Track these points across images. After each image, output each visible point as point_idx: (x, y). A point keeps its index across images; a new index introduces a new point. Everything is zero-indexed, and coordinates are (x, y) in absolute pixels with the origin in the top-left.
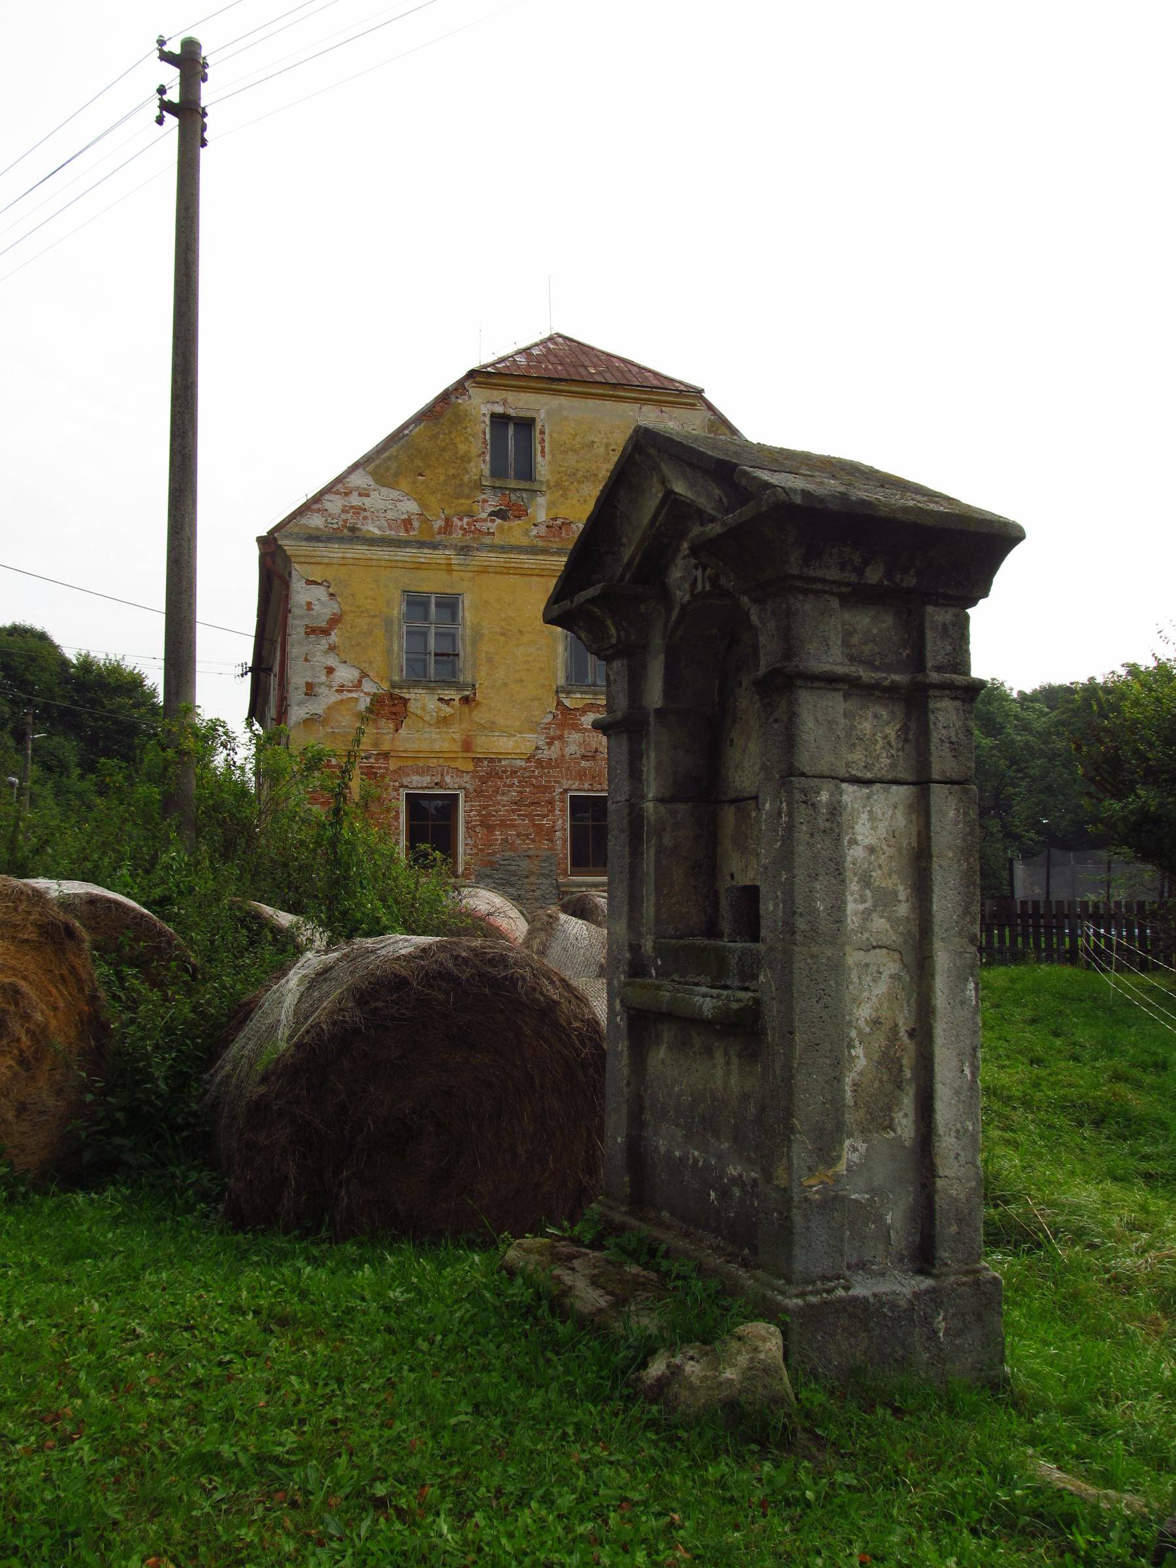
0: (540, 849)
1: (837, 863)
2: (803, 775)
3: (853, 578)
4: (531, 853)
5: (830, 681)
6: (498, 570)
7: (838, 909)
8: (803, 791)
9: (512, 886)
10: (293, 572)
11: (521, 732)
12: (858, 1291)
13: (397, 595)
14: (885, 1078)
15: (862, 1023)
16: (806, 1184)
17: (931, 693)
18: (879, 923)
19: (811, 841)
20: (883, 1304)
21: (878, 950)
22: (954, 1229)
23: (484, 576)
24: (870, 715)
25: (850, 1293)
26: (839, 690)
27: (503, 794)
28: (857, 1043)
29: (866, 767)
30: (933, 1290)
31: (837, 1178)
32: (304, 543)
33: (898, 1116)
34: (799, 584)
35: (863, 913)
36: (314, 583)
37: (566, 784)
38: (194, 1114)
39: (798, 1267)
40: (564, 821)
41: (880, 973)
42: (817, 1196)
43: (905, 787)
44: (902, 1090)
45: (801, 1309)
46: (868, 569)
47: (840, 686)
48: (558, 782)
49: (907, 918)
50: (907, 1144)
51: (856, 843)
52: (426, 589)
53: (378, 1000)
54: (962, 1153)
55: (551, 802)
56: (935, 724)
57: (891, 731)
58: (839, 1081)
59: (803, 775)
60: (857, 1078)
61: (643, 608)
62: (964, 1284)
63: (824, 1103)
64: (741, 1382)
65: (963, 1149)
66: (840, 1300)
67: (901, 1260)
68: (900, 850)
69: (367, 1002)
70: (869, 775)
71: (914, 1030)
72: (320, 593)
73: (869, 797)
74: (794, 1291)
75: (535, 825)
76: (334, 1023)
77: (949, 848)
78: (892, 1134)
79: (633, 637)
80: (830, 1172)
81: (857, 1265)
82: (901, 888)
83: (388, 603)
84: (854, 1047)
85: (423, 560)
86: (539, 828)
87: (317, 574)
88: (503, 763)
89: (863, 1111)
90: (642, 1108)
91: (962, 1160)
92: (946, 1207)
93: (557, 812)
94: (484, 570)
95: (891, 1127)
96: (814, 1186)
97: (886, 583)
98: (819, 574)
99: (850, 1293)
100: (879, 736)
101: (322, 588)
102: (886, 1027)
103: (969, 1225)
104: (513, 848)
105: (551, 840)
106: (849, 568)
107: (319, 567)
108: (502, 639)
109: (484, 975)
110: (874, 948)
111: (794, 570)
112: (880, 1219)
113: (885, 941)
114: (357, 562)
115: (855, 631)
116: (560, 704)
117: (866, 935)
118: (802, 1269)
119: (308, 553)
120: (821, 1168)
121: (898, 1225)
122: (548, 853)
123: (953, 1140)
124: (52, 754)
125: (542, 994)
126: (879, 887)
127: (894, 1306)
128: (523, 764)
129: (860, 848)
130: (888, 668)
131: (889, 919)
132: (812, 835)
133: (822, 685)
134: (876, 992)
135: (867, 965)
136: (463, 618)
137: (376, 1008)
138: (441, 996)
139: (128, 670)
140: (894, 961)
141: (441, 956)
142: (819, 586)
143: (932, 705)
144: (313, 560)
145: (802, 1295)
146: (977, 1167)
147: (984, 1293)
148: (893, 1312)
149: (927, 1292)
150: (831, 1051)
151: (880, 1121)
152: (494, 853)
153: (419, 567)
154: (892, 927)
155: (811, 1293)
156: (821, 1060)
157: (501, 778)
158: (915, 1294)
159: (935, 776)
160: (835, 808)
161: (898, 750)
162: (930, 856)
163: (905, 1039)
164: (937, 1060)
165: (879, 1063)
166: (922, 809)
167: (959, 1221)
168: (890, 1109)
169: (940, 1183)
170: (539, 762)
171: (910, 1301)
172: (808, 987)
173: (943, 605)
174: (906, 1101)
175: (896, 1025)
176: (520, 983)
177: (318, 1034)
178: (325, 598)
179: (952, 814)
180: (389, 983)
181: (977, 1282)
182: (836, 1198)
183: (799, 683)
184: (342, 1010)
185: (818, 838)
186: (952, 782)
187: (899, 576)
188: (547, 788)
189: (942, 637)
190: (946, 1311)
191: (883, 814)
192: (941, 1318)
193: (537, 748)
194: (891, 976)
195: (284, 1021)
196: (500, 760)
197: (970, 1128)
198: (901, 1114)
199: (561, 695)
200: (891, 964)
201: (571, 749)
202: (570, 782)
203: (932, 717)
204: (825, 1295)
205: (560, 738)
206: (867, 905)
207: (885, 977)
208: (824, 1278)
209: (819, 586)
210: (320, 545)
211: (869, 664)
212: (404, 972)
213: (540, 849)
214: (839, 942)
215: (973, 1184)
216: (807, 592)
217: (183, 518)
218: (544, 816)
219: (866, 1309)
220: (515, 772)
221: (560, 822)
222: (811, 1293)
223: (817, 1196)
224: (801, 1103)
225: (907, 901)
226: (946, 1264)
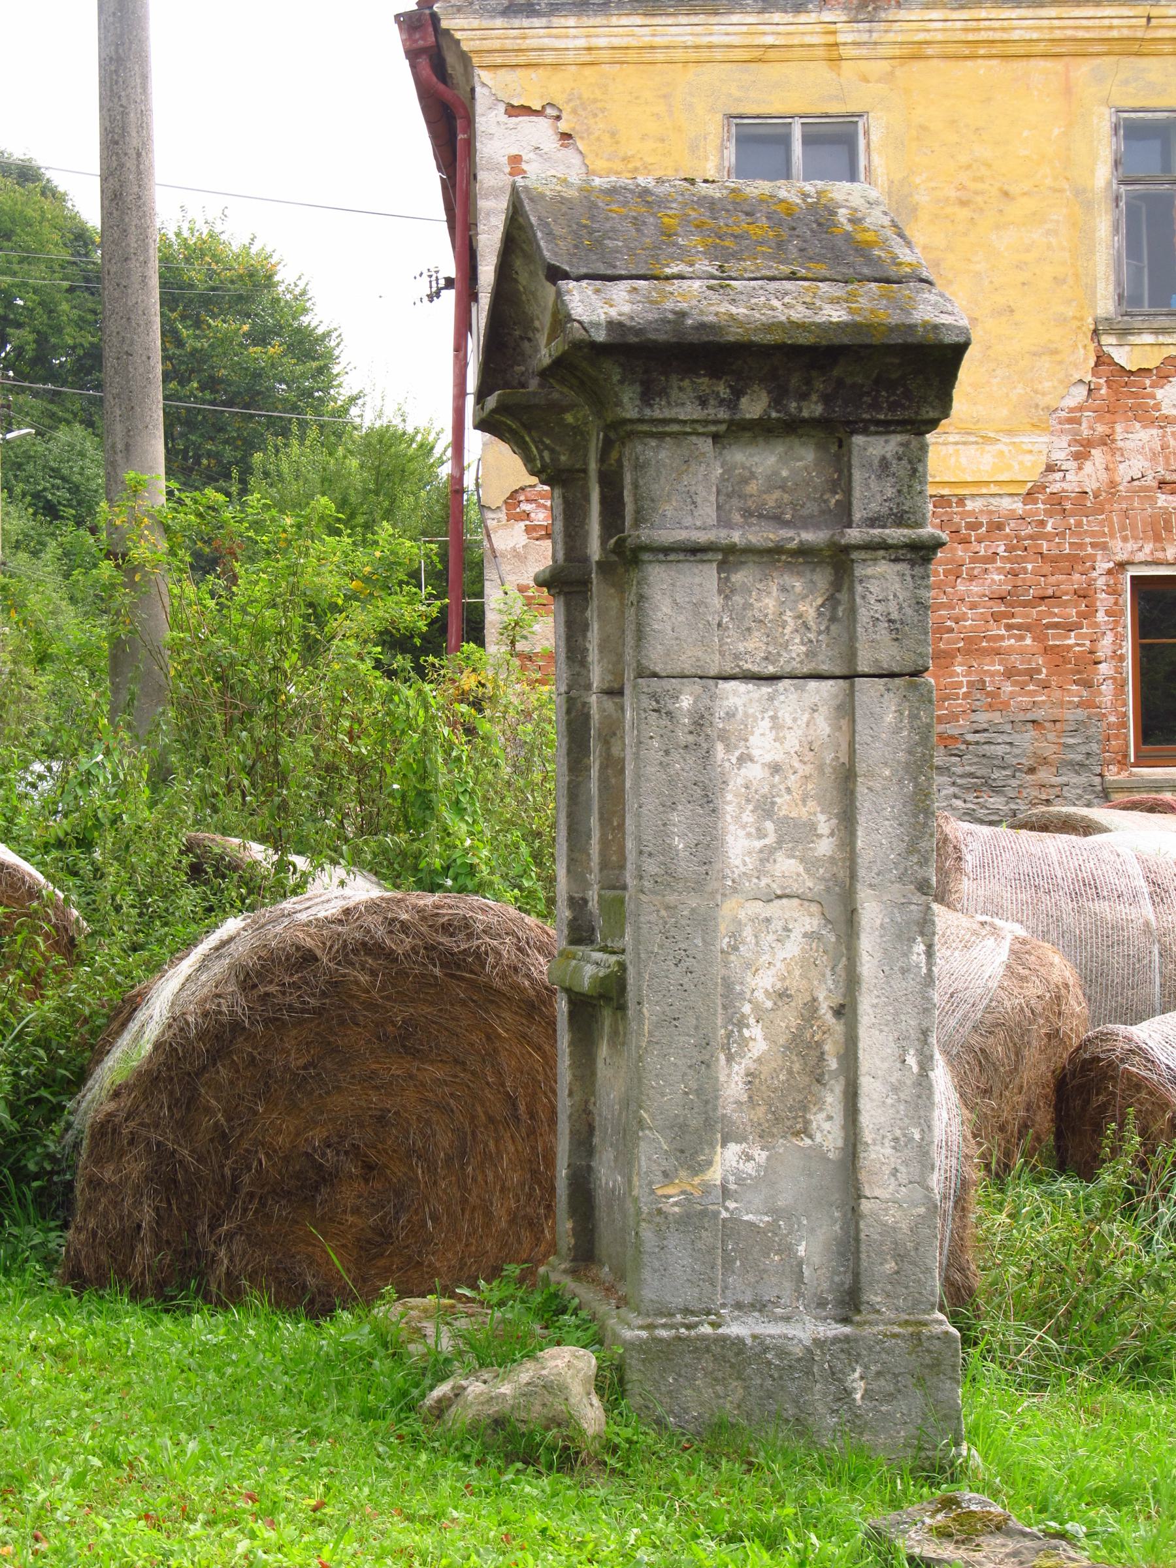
0: (1061, 704)
1: (705, 789)
2: (655, 675)
3: (723, 414)
4: (1039, 714)
5: (695, 551)
6: (951, 49)
7: (708, 847)
8: (654, 696)
9: (997, 790)
10: (479, 90)
11: (1010, 432)
12: (734, 1330)
13: (714, 128)
14: (797, 1067)
15: (760, 995)
16: (659, 1192)
17: (855, 555)
18: (787, 866)
19: (665, 760)
20: (766, 1349)
21: (784, 901)
22: (890, 1266)
23: (917, 65)
24: (775, 589)
25: (720, 1331)
26: (710, 561)
27: (972, 578)
28: (752, 1021)
29: (766, 658)
30: (847, 1339)
31: (707, 1189)
32: (499, 22)
33: (818, 1120)
34: (645, 428)
35: (761, 851)
36: (526, 110)
37: (1122, 550)
38: (51, 1157)
39: (648, 1294)
40: (1119, 638)
41: (789, 930)
42: (676, 1209)
43: (831, 682)
44: (824, 1085)
45: (644, 1342)
46: (744, 400)
47: (710, 556)
48: (1104, 547)
49: (832, 857)
50: (831, 1155)
51: (752, 760)
52: (776, 108)
53: (271, 982)
54: (903, 1169)
55: (1084, 595)
56: (864, 597)
57: (809, 609)
58: (708, 1066)
59: (655, 675)
60: (753, 1066)
61: (569, 418)
62: (895, 1336)
63: (686, 1093)
64: (514, 1398)
65: (906, 1163)
66: (703, 1338)
67: (822, 1304)
68: (821, 768)
69: (255, 986)
70: (771, 669)
71: (842, 1006)
72: (540, 131)
73: (771, 698)
74: (640, 1322)
75: (1047, 650)
76: (205, 1014)
77: (886, 764)
78: (808, 1141)
79: (563, 458)
80: (697, 1181)
81: (753, 1305)
82: (822, 818)
83: (694, 148)
84: (748, 1026)
85: (769, 40)
86: (1058, 656)
87: (528, 88)
88: (970, 505)
89: (763, 1109)
90: (591, 1129)
91: (903, 1177)
92: (877, 1237)
93: (1101, 617)
94: (915, 53)
95: (806, 1131)
96: (672, 1196)
97: (774, 415)
98: (667, 414)
99: (720, 1331)
100: (788, 616)
101: (543, 123)
102: (799, 1001)
103: (915, 1264)
104: (995, 702)
105: (1088, 684)
106: (712, 402)
107: (532, 74)
108: (964, 213)
109: (434, 948)
110: (779, 897)
111: (631, 413)
112: (787, 1250)
113: (795, 888)
114: (621, 56)
115: (753, 476)
116: (1102, 360)
117: (764, 881)
118: (654, 1298)
119: (509, 44)
120: (683, 1173)
121: (816, 1260)
122: (1081, 714)
123: (888, 1151)
124: (55, 472)
125: (528, 976)
126: (786, 817)
127: (782, 1353)
128: (1018, 507)
129: (758, 767)
130: (804, 522)
131: (802, 860)
132: (667, 752)
133: (681, 557)
134: (781, 955)
135: (768, 920)
136: (868, 169)
137: (267, 994)
138: (364, 979)
139: (236, 248)
140: (811, 915)
141: (370, 921)
142: (675, 428)
143: (859, 571)
144: (521, 59)
145: (650, 1327)
146: (929, 1189)
147: (928, 1351)
148: (781, 1359)
149: (836, 1340)
150: (696, 1028)
151: (789, 1123)
152: (953, 717)
153: (761, 56)
154: (807, 870)
155: (664, 1326)
156: (682, 1039)
157: (966, 541)
158: (816, 1341)
159: (863, 668)
160: (702, 717)
161: (820, 633)
162: (856, 776)
163: (829, 1018)
164: (861, 1045)
165: (788, 1048)
166: (847, 710)
167: (900, 1257)
168: (805, 1109)
169: (866, 1206)
170: (1057, 502)
171: (807, 1349)
172: (661, 947)
173: (877, 433)
174: (829, 1099)
175: (815, 1000)
176: (491, 960)
177: (181, 1030)
178: (550, 143)
179: (890, 718)
180: (287, 959)
181: (917, 1336)
182: (704, 1213)
183: (646, 556)
184: (218, 996)
185: (675, 755)
186: (892, 675)
187: (794, 405)
188: (1074, 562)
189: (879, 477)
190: (866, 1367)
191: (795, 720)
192: (857, 1375)
193: (1050, 468)
194: (805, 935)
195: (156, 1018)
196: (961, 500)
197: (917, 1137)
198: (821, 1116)
199: (1106, 340)
200: (807, 919)
201: (1133, 466)
202: (1131, 545)
203: (859, 589)
204: (683, 1330)
205: (1106, 441)
206: (767, 841)
207: (797, 935)
208: (687, 1311)
209: (675, 428)
210: (536, 22)
211: (777, 519)
212: (309, 943)
213: (1061, 704)
214: (709, 889)
215: (922, 1210)
216: (661, 436)
217: (124, 114)
218: (1069, 628)
219: (740, 1353)
220: (1000, 527)
221: (1108, 640)
222: (664, 1326)
223: (676, 1209)
224: (651, 1092)
225: (832, 834)
226: (878, 1312)
